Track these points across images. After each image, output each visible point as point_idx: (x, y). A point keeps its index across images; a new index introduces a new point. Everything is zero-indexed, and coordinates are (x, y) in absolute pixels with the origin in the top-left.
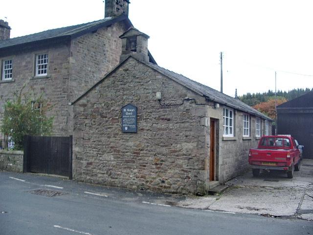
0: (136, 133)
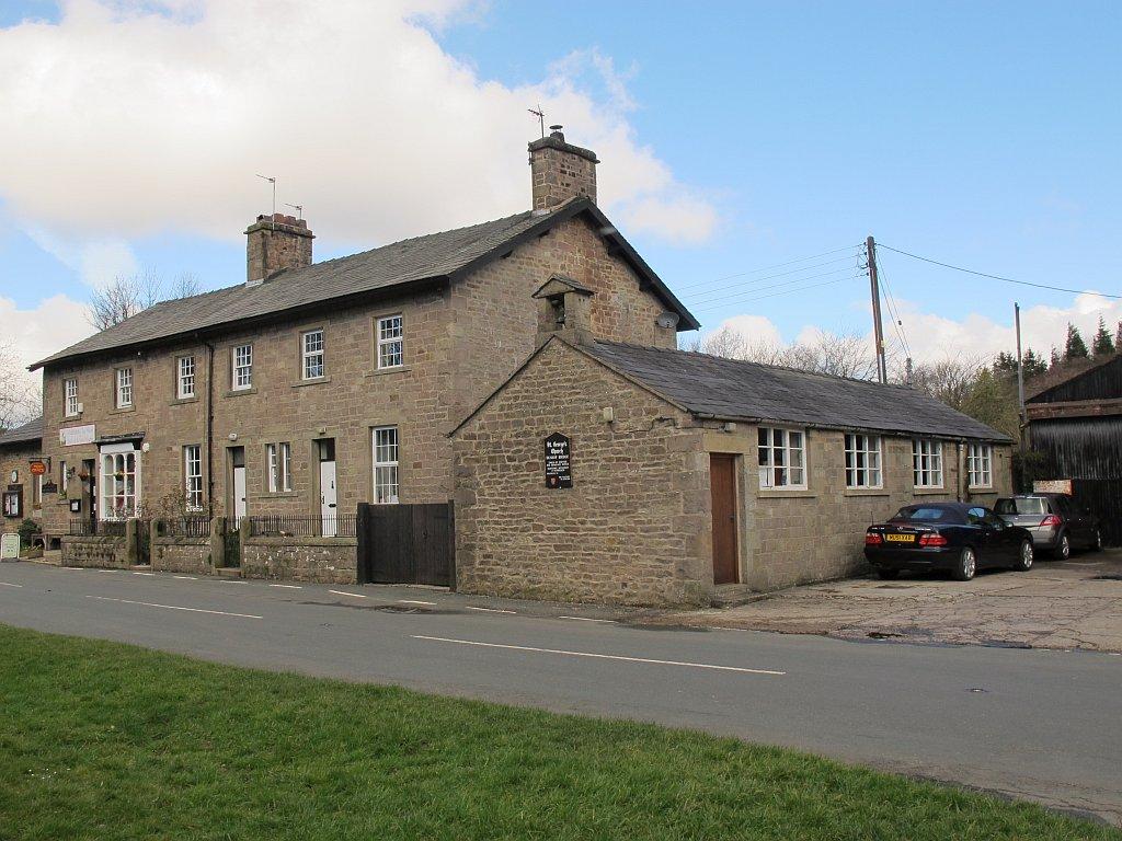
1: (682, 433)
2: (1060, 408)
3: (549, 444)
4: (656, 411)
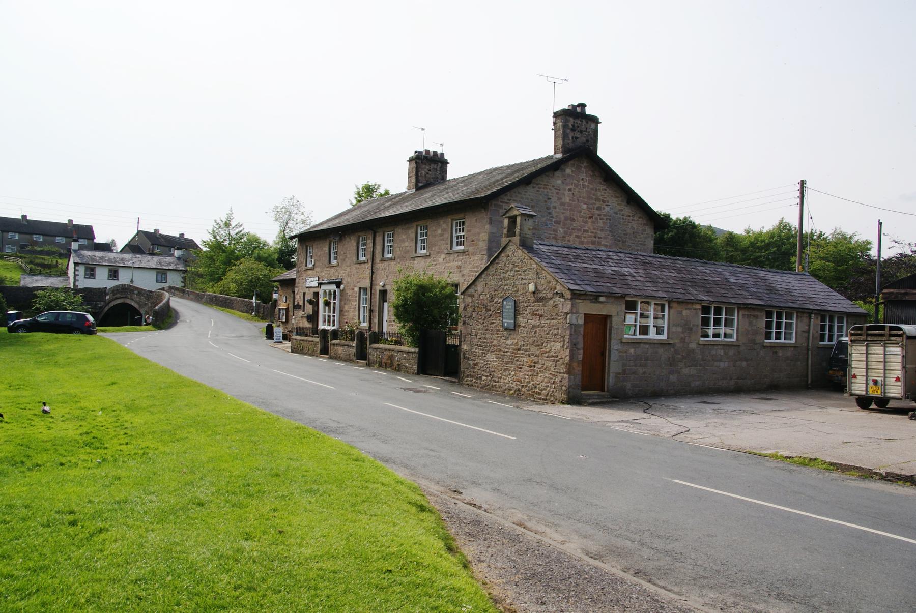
0: (514, 329)
2: (906, 294)
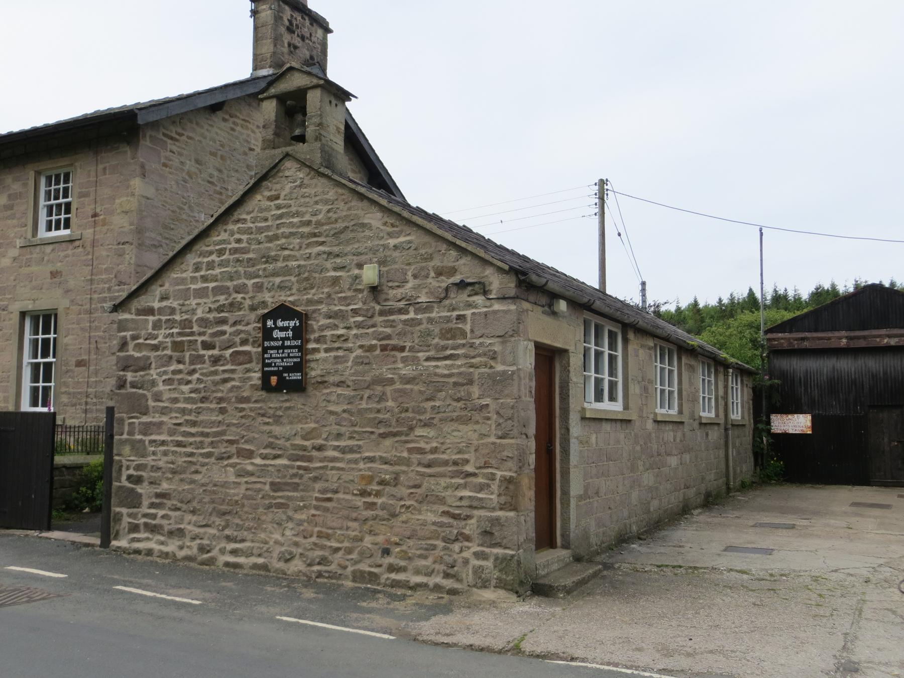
1: (497, 306)
2: (803, 339)
3: (270, 323)
4: (453, 271)
